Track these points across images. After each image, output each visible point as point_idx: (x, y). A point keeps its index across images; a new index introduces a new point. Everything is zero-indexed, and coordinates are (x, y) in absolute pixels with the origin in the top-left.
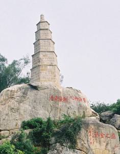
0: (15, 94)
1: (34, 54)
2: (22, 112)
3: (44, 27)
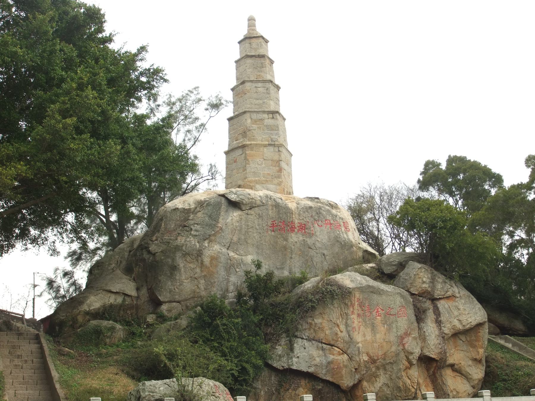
0: (192, 216)
1: (232, 115)
2: (207, 261)
3: (256, 49)
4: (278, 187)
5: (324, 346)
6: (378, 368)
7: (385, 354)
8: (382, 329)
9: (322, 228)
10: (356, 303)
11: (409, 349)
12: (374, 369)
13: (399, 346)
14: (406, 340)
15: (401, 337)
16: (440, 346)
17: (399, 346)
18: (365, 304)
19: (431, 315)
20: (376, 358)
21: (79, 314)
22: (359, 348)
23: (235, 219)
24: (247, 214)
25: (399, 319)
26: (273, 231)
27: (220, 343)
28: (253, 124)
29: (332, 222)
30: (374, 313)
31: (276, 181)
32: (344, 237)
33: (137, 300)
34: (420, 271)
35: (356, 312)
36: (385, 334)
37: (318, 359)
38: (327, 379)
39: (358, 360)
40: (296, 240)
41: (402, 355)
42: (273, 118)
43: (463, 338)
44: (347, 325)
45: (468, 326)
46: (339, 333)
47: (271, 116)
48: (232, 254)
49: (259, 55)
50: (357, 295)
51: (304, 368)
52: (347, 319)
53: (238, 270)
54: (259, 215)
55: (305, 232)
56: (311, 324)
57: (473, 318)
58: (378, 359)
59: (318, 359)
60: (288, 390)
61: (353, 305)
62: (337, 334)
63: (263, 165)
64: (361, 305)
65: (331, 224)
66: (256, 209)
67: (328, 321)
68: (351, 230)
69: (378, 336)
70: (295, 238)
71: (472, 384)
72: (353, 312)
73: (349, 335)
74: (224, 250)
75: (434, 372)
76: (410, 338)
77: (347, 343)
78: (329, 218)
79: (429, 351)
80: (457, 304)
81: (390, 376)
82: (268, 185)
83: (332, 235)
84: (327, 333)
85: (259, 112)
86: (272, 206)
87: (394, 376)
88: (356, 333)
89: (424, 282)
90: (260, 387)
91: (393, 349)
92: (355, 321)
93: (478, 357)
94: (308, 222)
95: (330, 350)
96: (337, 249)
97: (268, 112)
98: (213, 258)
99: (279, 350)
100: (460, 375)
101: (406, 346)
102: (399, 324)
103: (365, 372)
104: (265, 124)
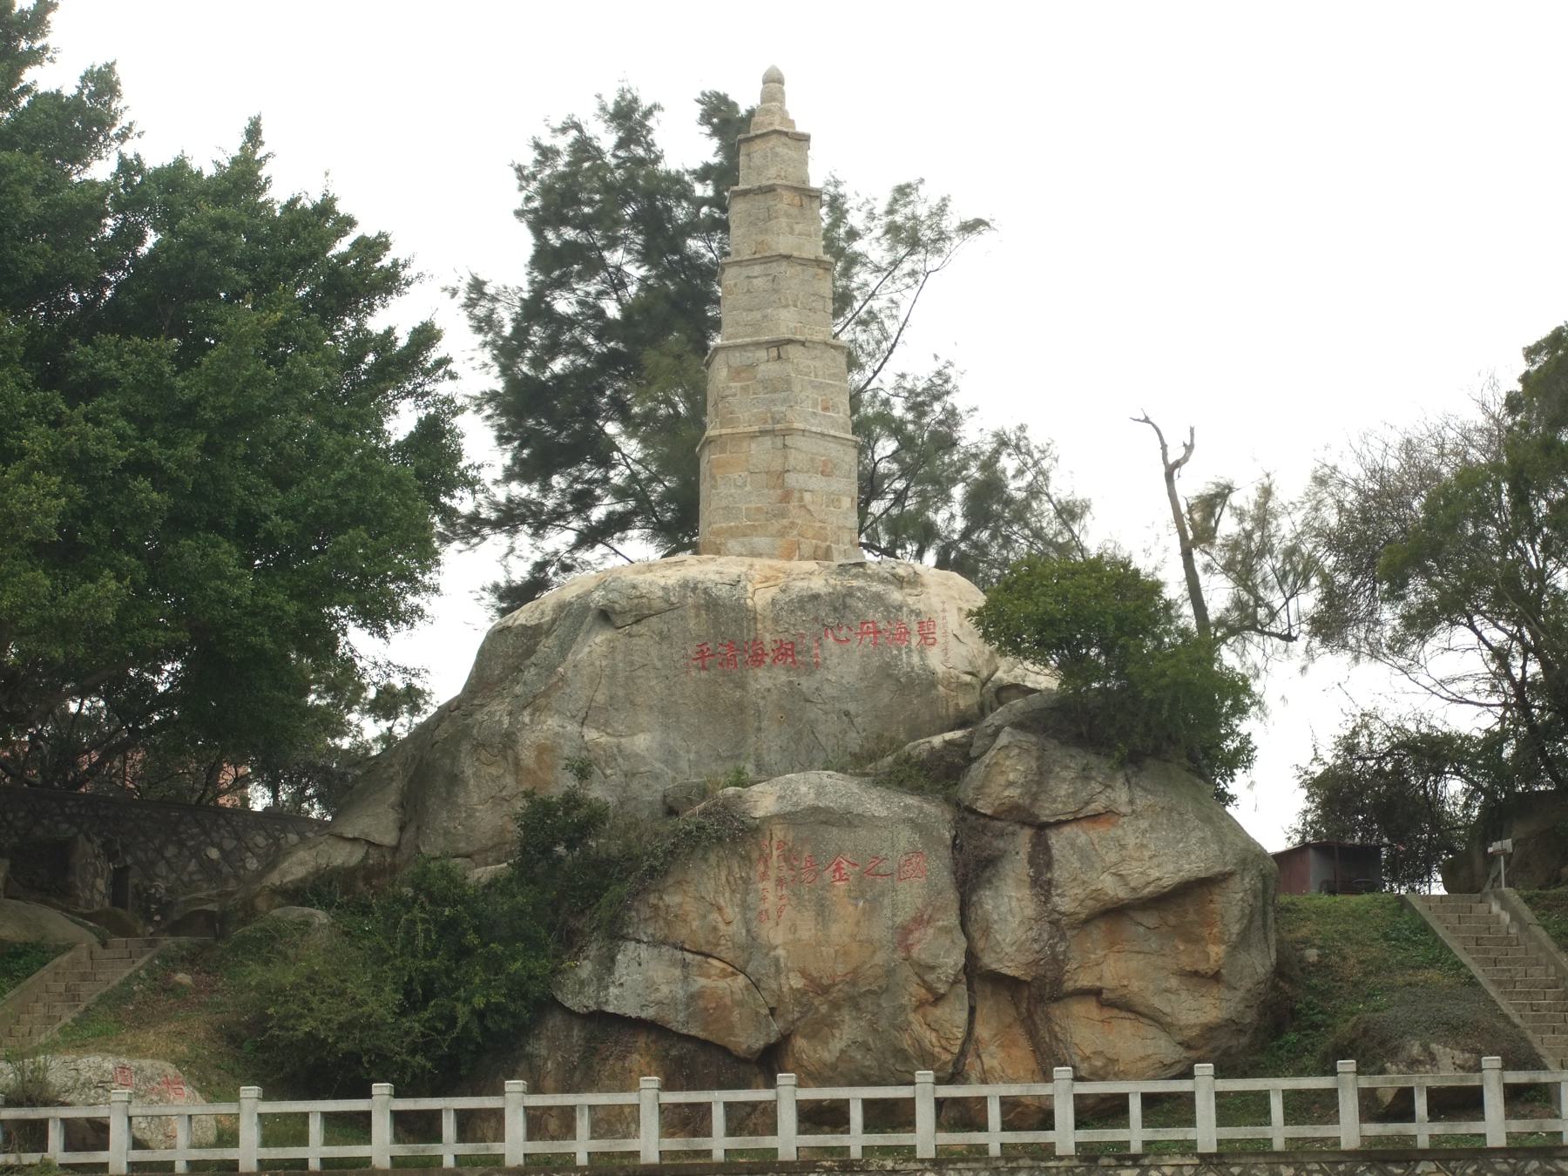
2: (528, 757)
4: (779, 542)
5: (689, 956)
6: (835, 1006)
7: (855, 971)
9: (848, 645)
10: (775, 853)
11: (923, 956)
12: (824, 1009)
13: (894, 950)
14: (917, 935)
15: (904, 928)
16: (1036, 947)
17: (894, 950)
18: (800, 853)
19: (1017, 867)
20: (825, 982)
21: (258, 895)
22: (777, 960)
23: (599, 650)
24: (630, 635)
25: (901, 884)
26: (704, 668)
28: (733, 380)
29: (881, 626)
30: (828, 875)
31: (776, 525)
32: (909, 663)
33: (393, 855)
34: (1002, 753)
35: (772, 874)
36: (857, 923)
37: (665, 989)
38: (693, 1033)
39: (775, 986)
40: (769, 684)
41: (907, 971)
42: (779, 357)
43: (1150, 919)
44: (744, 906)
46: (722, 926)
47: (774, 352)
48: (591, 735)
49: (760, 188)
50: (779, 833)
51: (631, 1009)
52: (746, 892)
53: (609, 772)
54: (661, 633)
55: (794, 662)
56: (656, 908)
58: (834, 985)
59: (665, 989)
60: (607, 1059)
61: (765, 858)
62: (715, 929)
63: (748, 488)
64: (789, 857)
65: (877, 632)
66: (654, 619)
67: (703, 899)
68: (940, 640)
69: (835, 929)
70: (766, 680)
71: (1178, 1038)
72: (764, 873)
73: (748, 931)
74: (572, 728)
76: (931, 931)
77: (743, 948)
78: (874, 615)
79: (1000, 961)
80: (1120, 832)
81: (871, 1024)
82: (756, 539)
83: (876, 661)
84: (693, 927)
85: (748, 345)
86: (697, 607)
87: (883, 1024)
89: (1010, 784)
90: (544, 1052)
91: (880, 958)
92: (769, 893)
93: (1202, 967)
94: (802, 636)
95: (700, 967)
96: (885, 697)
97: (767, 342)
98: (542, 750)
99: (586, 969)
100: (1132, 1016)
101: (915, 952)
102: (901, 897)
103: (796, 1015)
104: (759, 376)
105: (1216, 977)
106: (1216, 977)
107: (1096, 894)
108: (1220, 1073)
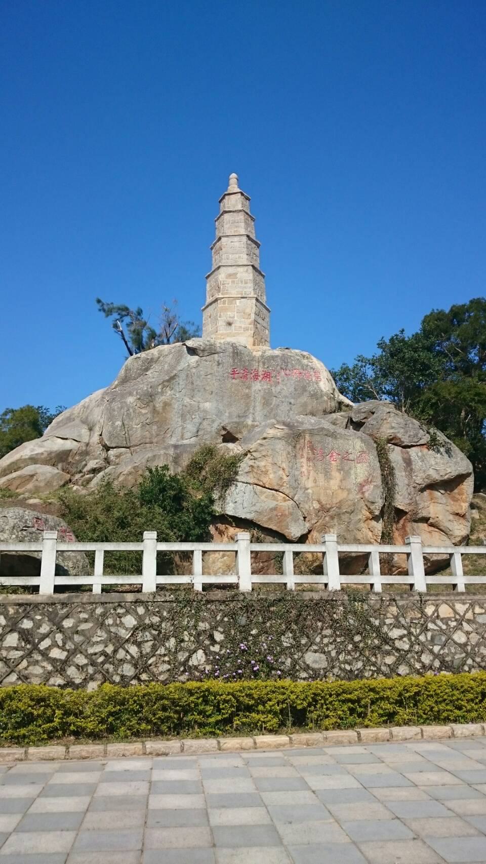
6: (332, 518)
8: (337, 476)
27: (9, 424)
41: (362, 504)
45: (446, 477)
57: (453, 468)
62: (281, 478)
75: (403, 525)
88: (304, 478)
93: (460, 512)
101: (366, 495)
105: (463, 516)
106: (463, 516)
107: (428, 477)
108: (162, 538)
